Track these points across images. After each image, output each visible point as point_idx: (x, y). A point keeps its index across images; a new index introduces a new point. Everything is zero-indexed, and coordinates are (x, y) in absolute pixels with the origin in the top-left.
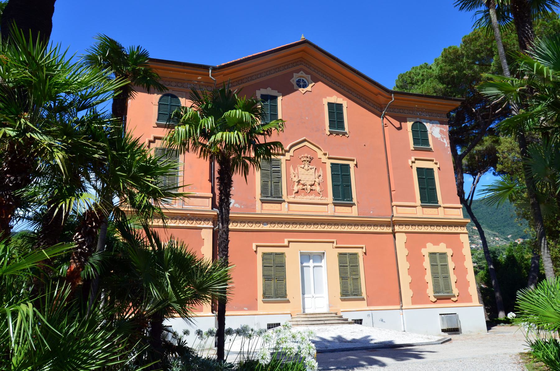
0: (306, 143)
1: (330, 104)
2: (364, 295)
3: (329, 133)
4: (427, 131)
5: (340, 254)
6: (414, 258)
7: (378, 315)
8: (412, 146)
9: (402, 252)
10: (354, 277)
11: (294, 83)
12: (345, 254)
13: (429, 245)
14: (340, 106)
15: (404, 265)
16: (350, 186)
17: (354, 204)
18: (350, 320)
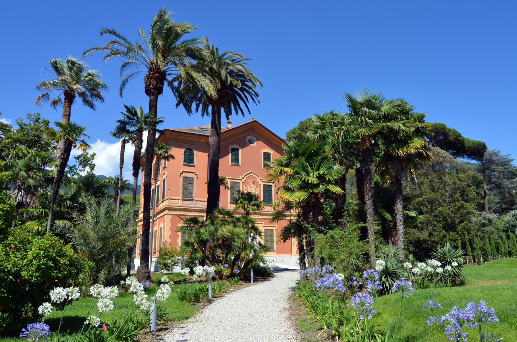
0: (252, 174)
1: (264, 153)
2: (275, 249)
4: (193, 155)
7: (281, 258)
8: (182, 163)
11: (248, 142)
14: (269, 154)
16: (271, 196)
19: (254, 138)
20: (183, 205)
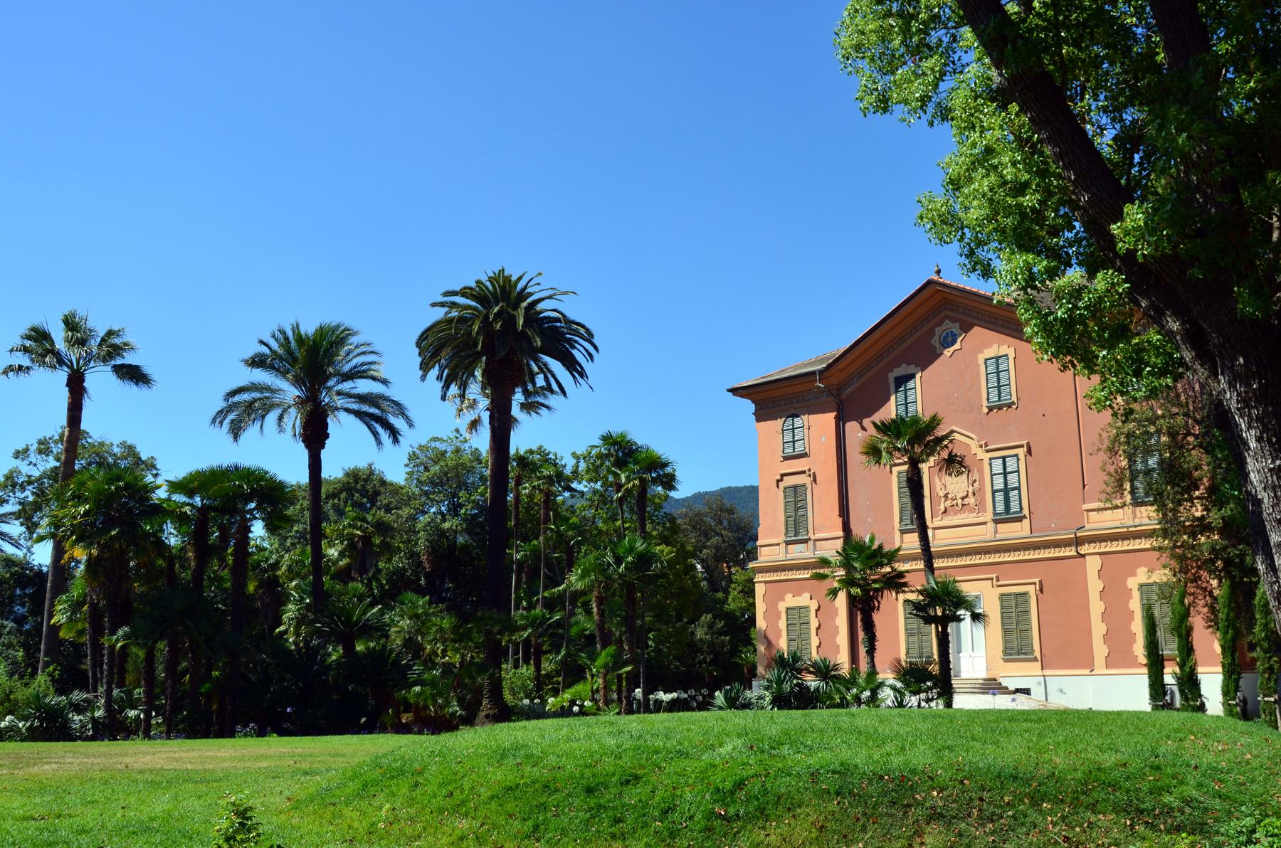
3: (986, 410)
5: (1002, 595)
6: (1114, 594)
9: (1095, 586)
10: (1023, 628)
12: (1010, 595)
13: (789, 597)
15: (1096, 607)
17: (1025, 517)
18: (1012, 688)
19: (955, 328)
20: (999, 536)
